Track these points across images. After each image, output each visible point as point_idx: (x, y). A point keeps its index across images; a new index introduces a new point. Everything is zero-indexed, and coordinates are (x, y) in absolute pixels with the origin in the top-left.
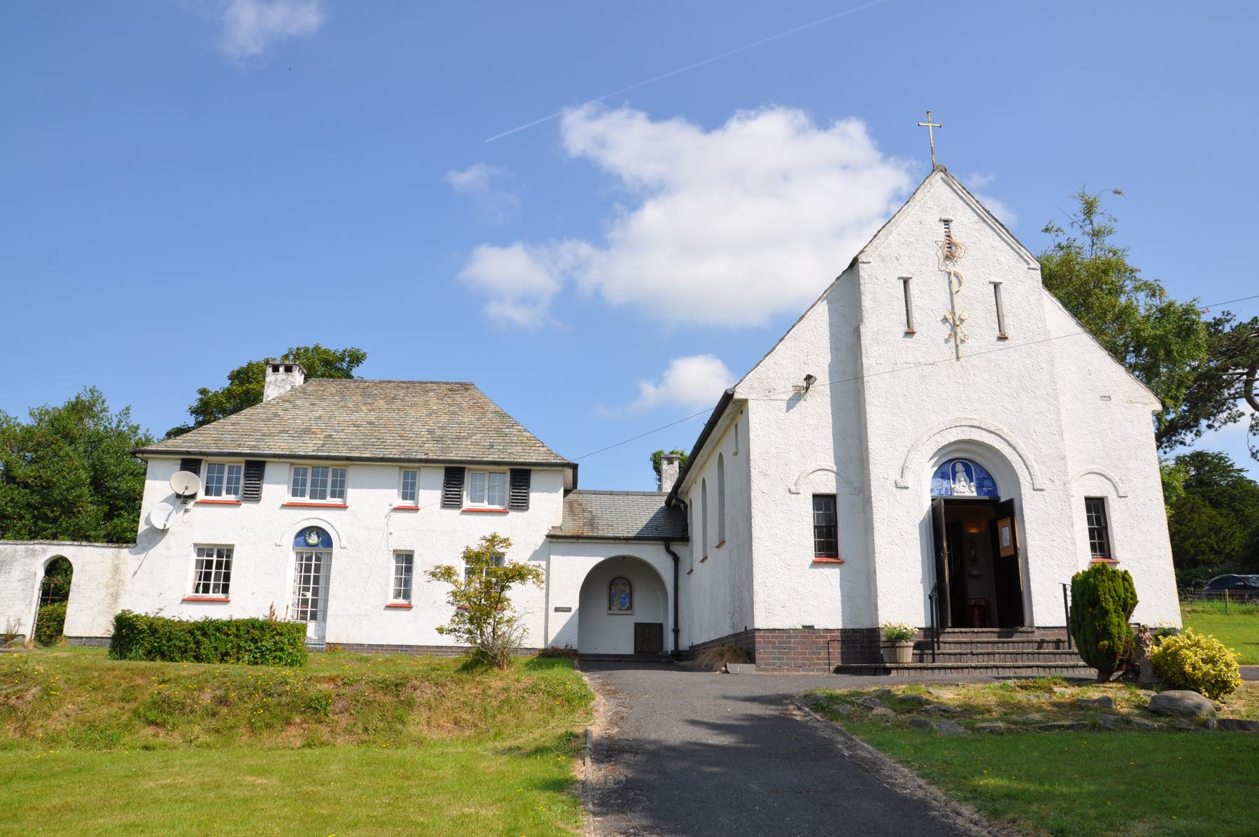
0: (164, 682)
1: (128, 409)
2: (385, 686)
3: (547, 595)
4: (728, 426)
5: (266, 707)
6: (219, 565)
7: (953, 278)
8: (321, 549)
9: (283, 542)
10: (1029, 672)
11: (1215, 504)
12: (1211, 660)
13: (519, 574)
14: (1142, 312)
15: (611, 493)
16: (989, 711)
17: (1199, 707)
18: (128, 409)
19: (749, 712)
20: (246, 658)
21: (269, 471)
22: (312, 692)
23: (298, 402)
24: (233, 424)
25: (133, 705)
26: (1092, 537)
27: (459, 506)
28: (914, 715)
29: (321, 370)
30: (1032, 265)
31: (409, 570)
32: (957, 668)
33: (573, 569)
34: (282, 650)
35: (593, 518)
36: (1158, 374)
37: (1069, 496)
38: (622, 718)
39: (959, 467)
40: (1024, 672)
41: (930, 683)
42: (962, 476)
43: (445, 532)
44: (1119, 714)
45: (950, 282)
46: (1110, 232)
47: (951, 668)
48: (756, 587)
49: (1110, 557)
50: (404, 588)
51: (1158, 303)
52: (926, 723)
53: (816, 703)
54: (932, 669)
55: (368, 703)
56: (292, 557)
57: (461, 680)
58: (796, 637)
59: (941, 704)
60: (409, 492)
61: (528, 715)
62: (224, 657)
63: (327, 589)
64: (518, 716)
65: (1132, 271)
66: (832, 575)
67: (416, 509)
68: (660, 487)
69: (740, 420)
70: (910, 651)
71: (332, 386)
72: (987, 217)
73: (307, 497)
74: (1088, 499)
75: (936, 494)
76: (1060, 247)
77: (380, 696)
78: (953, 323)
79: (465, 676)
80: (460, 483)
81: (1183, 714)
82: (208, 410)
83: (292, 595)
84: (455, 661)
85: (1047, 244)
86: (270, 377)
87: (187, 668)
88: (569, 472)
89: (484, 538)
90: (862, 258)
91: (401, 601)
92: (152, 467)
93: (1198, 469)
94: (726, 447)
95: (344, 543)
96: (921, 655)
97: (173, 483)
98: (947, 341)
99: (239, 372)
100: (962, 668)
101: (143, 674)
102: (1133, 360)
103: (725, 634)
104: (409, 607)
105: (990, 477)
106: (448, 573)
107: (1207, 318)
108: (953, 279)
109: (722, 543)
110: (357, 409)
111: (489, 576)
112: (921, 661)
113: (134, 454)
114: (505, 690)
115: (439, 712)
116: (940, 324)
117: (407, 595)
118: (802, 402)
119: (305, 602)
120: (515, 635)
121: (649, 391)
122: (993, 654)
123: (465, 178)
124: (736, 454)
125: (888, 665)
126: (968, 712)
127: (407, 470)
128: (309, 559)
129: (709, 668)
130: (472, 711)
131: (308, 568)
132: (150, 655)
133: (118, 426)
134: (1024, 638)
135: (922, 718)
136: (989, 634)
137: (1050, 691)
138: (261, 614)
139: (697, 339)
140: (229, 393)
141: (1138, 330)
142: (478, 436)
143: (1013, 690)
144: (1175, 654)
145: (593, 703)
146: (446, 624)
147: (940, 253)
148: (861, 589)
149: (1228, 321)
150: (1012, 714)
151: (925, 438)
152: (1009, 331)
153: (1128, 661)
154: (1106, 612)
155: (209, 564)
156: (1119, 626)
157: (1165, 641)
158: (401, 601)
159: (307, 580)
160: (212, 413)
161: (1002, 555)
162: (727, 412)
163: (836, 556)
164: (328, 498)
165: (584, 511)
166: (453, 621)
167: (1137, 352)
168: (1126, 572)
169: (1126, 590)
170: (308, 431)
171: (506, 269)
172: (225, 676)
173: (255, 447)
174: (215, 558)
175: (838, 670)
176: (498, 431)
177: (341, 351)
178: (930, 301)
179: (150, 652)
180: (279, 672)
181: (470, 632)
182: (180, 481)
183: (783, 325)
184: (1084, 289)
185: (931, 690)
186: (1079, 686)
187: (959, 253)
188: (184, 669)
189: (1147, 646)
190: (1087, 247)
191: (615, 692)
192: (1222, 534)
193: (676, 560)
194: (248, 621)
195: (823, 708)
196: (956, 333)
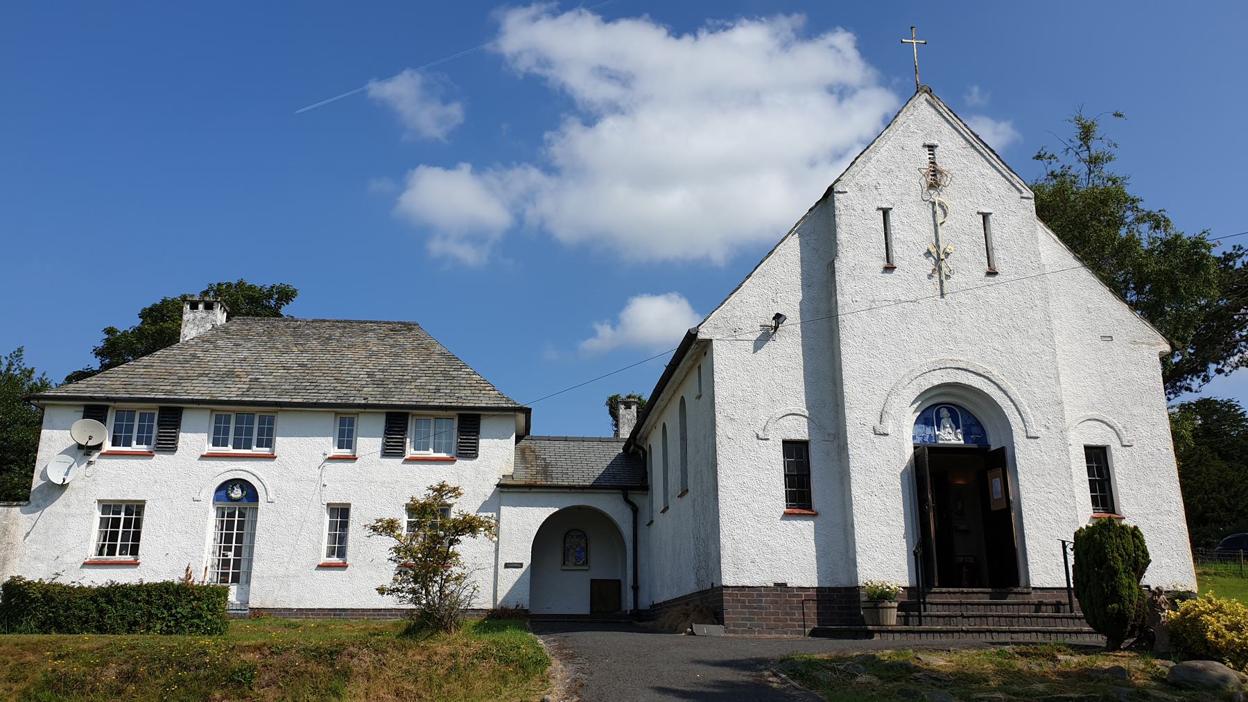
0: (61, 657)
1: (20, 350)
2: (318, 655)
3: (497, 550)
4: (691, 368)
5: (181, 682)
6: (127, 523)
7: (937, 208)
8: (245, 504)
9: (202, 497)
10: (1027, 638)
11: (1225, 457)
12: (1235, 627)
13: (469, 526)
14: (1145, 245)
15: (566, 439)
16: (986, 681)
17: (1225, 679)
18: (20, 350)
19: (715, 678)
20: (158, 626)
21: (187, 418)
22: (235, 663)
23: (220, 343)
24: (145, 367)
25: (22, 686)
26: (1092, 490)
27: (401, 455)
28: (902, 684)
29: (245, 308)
30: (1025, 195)
31: (344, 525)
32: (946, 632)
33: (524, 523)
34: (200, 617)
35: (546, 466)
36: (1163, 313)
37: (1066, 444)
38: (582, 685)
39: (944, 412)
40: (1027, 638)
41: (919, 649)
42: (947, 422)
43: (386, 483)
44: (1134, 686)
45: (934, 213)
46: (1110, 159)
47: (940, 632)
48: (723, 540)
49: (1114, 512)
50: (339, 546)
51: (1163, 235)
52: (916, 693)
53: (789, 666)
54: (920, 632)
55: (299, 674)
56: (212, 513)
57: (404, 646)
58: (768, 596)
59: (933, 671)
60: (346, 440)
61: (479, 684)
62: (132, 627)
63: (251, 548)
64: (467, 686)
65: (1133, 201)
66: (806, 527)
67: (353, 459)
68: (617, 433)
69: (703, 362)
70: (894, 612)
71: (258, 326)
72: (976, 142)
73: (230, 447)
74: (1088, 449)
75: (918, 441)
76: (1053, 175)
77: (312, 666)
78: (937, 257)
79: (408, 641)
80: (403, 430)
81: (1206, 688)
82: (116, 350)
83: (210, 556)
84: (395, 625)
85: (1040, 171)
86: (188, 314)
87: (89, 640)
88: (521, 417)
89: (431, 488)
90: (838, 187)
91: (335, 560)
92: (49, 414)
93: (1203, 417)
94: (689, 391)
95: (272, 496)
96: (907, 617)
97: (75, 432)
98: (930, 276)
99: (151, 309)
100: (953, 632)
101: (35, 648)
102: (1134, 298)
103: (689, 592)
104: (344, 566)
105: (978, 424)
106: (389, 527)
107: (1217, 252)
108: (938, 210)
109: (684, 492)
110: (287, 351)
111: (432, 534)
112: (906, 624)
113: (28, 400)
114: (453, 656)
115: (379, 682)
116: (923, 258)
117: (342, 553)
118: (771, 343)
119: (226, 563)
120: (465, 593)
121: (605, 331)
122: (986, 617)
123: (401, 90)
124: (699, 397)
125: (870, 627)
126: (962, 681)
127: (344, 419)
128: (232, 515)
129: (673, 630)
130: (416, 681)
131: (230, 525)
132: (43, 627)
133: (8, 370)
134: (1019, 599)
135: (912, 687)
136: (980, 595)
137: (1054, 659)
138: (176, 577)
139: (661, 277)
140: (139, 333)
141: (1140, 265)
142: (424, 379)
143: (1012, 657)
144: (1196, 619)
145: (549, 669)
146: (387, 582)
147: (923, 181)
148: (838, 543)
149: (1240, 256)
150: (1012, 683)
151: (907, 380)
152: (999, 266)
153: (1141, 628)
154: (1115, 572)
155: (116, 522)
156: (1130, 587)
157: (1182, 605)
158: (335, 560)
159: (228, 539)
160: (120, 355)
161: (993, 508)
162: (690, 353)
163: (809, 507)
164: (254, 447)
165: (537, 458)
166: (395, 580)
167: (1139, 289)
168: (1136, 528)
169: (1137, 547)
170: (231, 374)
171: (451, 198)
172: (133, 648)
173: (170, 391)
174: (122, 516)
175: (814, 633)
176: (445, 374)
177: (268, 287)
178: (912, 233)
179: (44, 624)
180: (197, 641)
181: (413, 591)
182: (82, 430)
183: (748, 260)
184: (1084, 220)
185: (920, 656)
186: (1086, 654)
187: (944, 181)
188: (85, 642)
189: (1163, 610)
190: (1083, 176)
191: (573, 656)
192: (1233, 490)
193: (635, 510)
194: (161, 585)
195: (802, 675)
196: (940, 268)
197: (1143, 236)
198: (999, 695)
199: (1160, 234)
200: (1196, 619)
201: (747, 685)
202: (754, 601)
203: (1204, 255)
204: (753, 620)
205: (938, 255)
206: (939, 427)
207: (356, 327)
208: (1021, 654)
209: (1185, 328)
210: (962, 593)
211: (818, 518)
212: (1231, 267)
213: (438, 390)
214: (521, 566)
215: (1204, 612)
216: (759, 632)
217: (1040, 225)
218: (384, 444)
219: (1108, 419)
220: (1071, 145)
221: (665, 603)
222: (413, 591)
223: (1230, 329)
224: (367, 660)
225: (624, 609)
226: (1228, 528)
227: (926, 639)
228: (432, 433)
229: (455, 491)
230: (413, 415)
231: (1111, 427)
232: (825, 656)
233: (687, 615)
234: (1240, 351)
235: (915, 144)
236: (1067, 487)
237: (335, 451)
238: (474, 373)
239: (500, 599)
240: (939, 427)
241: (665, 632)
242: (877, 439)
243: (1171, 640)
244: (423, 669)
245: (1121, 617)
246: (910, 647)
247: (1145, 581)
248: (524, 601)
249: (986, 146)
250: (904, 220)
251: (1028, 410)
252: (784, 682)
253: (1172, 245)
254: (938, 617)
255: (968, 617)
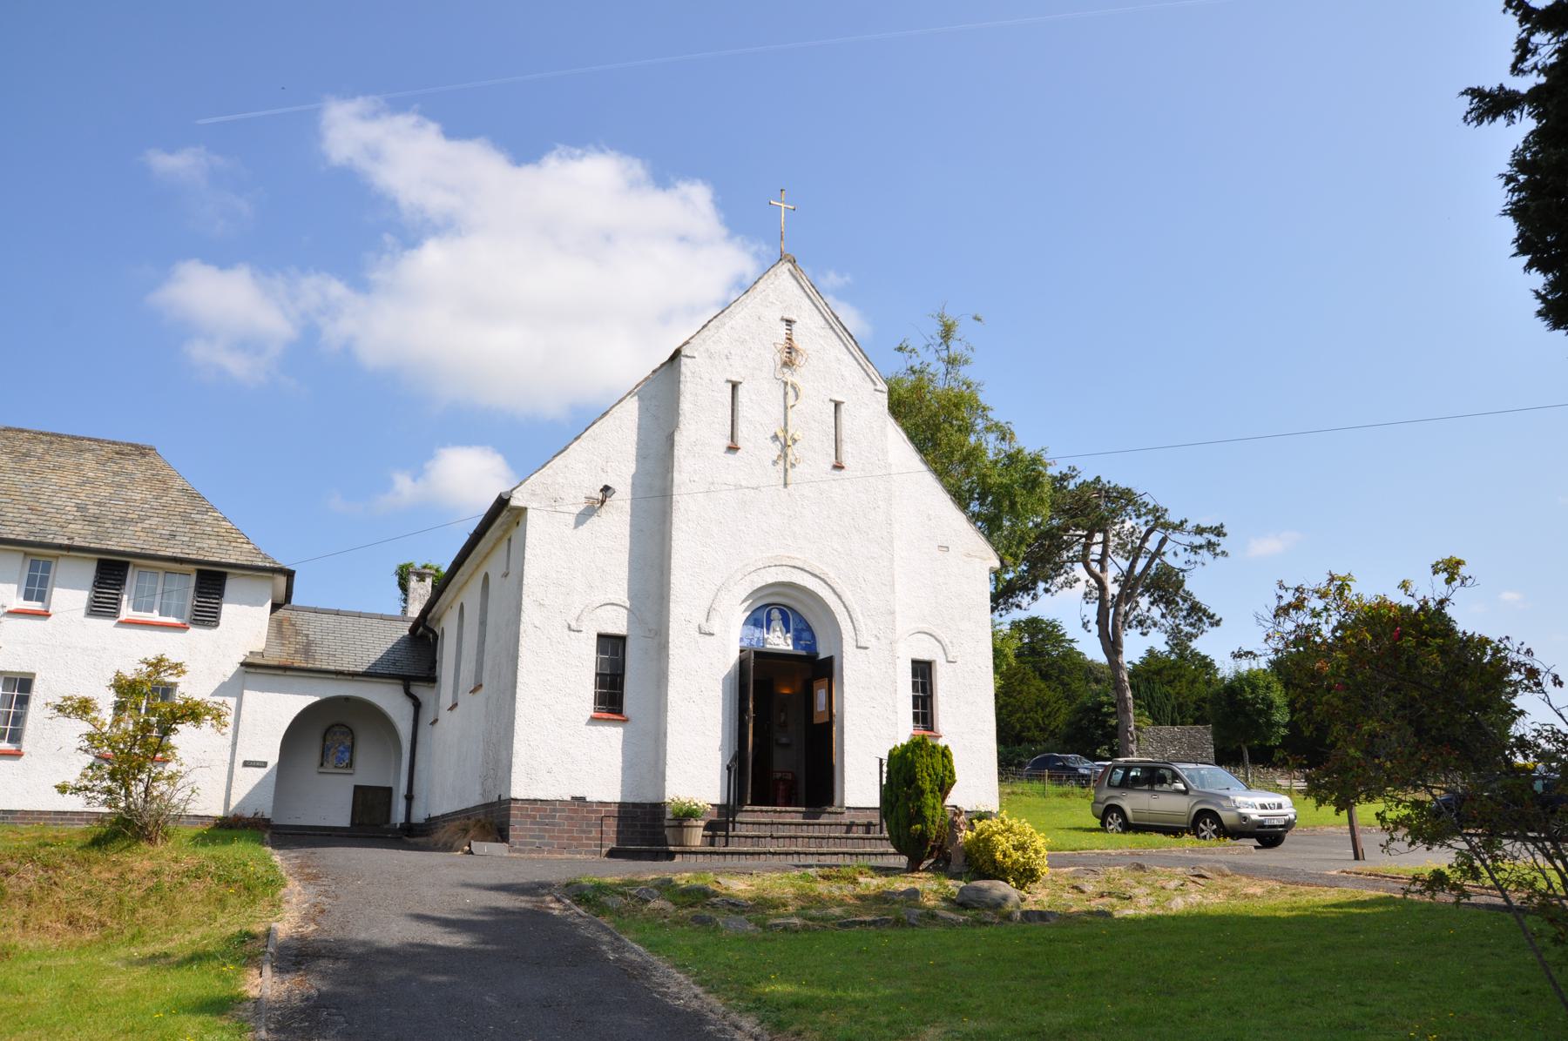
4: (500, 539)
11: (1045, 676)
13: (193, 713)
14: (991, 455)
15: (337, 613)
16: (785, 905)
17: (1005, 898)
26: (915, 706)
27: (114, 614)
31: (23, 701)
33: (273, 712)
35: (309, 644)
36: (1000, 528)
37: (895, 657)
38: (322, 911)
39: (776, 614)
40: (828, 860)
42: (777, 625)
46: (966, 362)
49: (932, 730)
52: (710, 919)
54: (724, 854)
57: (87, 860)
59: (731, 896)
60: (36, 588)
61: (186, 909)
64: (171, 911)
65: (984, 409)
66: (613, 735)
67: (45, 615)
68: (405, 610)
69: (514, 533)
70: (700, 832)
72: (835, 324)
78: (784, 442)
79: (94, 854)
80: (120, 582)
84: (84, 832)
85: (898, 365)
88: (281, 581)
89: (146, 662)
90: (686, 351)
93: (1031, 636)
94: (495, 566)
102: (977, 509)
105: (809, 628)
106: (84, 708)
107: (1053, 471)
109: (478, 687)
112: (712, 845)
114: (155, 873)
115: (44, 907)
116: (769, 442)
118: (595, 518)
120: (179, 795)
121: (404, 484)
124: (506, 575)
126: (761, 906)
129: (448, 848)
130: (99, 905)
136: (793, 815)
137: (855, 881)
141: (985, 475)
142: (154, 521)
143: (814, 880)
144: (988, 839)
145: (283, 891)
146: (72, 778)
147: (777, 358)
148: (647, 755)
152: (846, 460)
156: (934, 808)
157: (979, 825)
161: (816, 721)
162: (499, 521)
163: (620, 712)
165: (297, 633)
166: (84, 775)
167: (982, 499)
175: (612, 854)
176: (185, 517)
181: (109, 791)
184: (933, 422)
187: (799, 360)
190: (940, 376)
191: (316, 877)
193: (417, 705)
195: (588, 901)
198: (796, 921)
199: (1005, 446)
201: (524, 912)
202: (546, 817)
207: (68, 445)
209: (1018, 546)
213: (173, 536)
214: (264, 765)
216: (549, 852)
217: (891, 421)
218: (91, 600)
219: (941, 636)
222: (109, 791)
223: (1060, 548)
224: (31, 877)
228: (159, 591)
229: (178, 668)
230: (135, 566)
233: (465, 831)
235: (774, 316)
237: (20, 604)
238: (225, 519)
241: (439, 850)
244: (111, 889)
245: (922, 838)
247: (949, 801)
252: (567, 908)
253: (1013, 459)
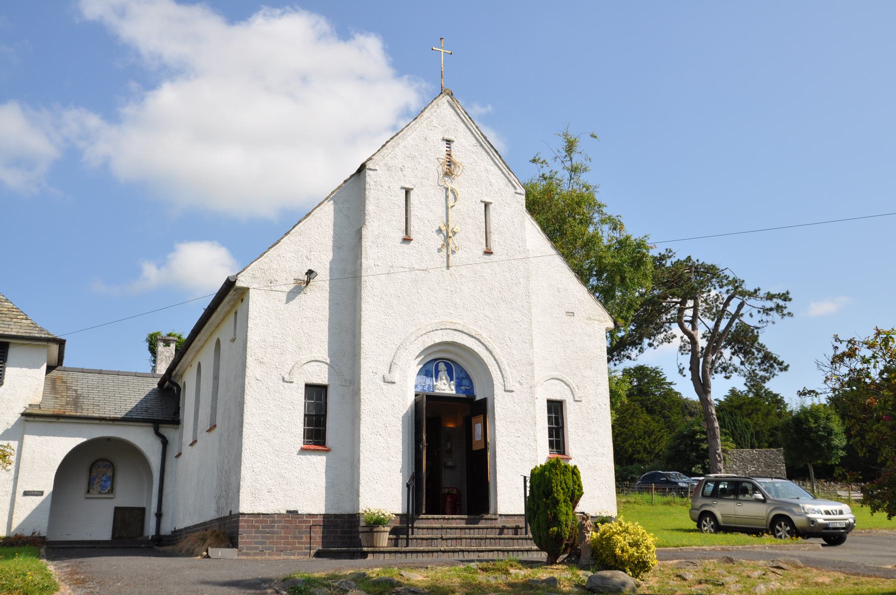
4: (228, 312)
7: (450, 193)
10: (490, 556)
11: (650, 411)
12: (635, 544)
14: (605, 242)
15: (100, 372)
26: (550, 435)
32: (427, 552)
35: (77, 397)
36: (613, 297)
37: (534, 398)
39: (442, 366)
40: (485, 556)
41: (402, 567)
42: (443, 375)
45: (447, 197)
46: (585, 170)
47: (422, 552)
49: (564, 453)
51: (618, 236)
54: (406, 552)
58: (280, 522)
59: (411, 585)
65: (600, 206)
66: (319, 461)
68: (154, 369)
70: (386, 536)
72: (484, 142)
75: (419, 390)
78: (447, 234)
85: (533, 173)
88: (55, 348)
90: (370, 165)
93: (639, 380)
94: (225, 333)
96: (396, 540)
98: (439, 250)
100: (432, 552)
102: (595, 283)
105: (468, 377)
107: (654, 253)
109: (213, 427)
112: (396, 545)
116: (435, 234)
118: (302, 295)
121: (150, 271)
122: (461, 539)
124: (233, 340)
125: (365, 549)
129: (190, 553)
136: (458, 521)
137: (507, 573)
141: (601, 257)
143: (476, 572)
144: (609, 539)
147: (440, 169)
148: (344, 477)
149: (669, 257)
151: (413, 337)
152: (494, 247)
153: (572, 546)
156: (567, 514)
157: (602, 528)
165: (68, 389)
167: (599, 275)
168: (575, 467)
169: (574, 482)
175: (318, 554)
178: (427, 212)
183: (291, 220)
184: (559, 216)
185: (403, 572)
186: (531, 568)
187: (457, 171)
189: (588, 532)
190: (566, 181)
191: (84, 581)
192: (653, 437)
193: (165, 442)
196: (448, 244)
197: (605, 234)
199: (616, 234)
200: (609, 539)
202: (267, 527)
203: (644, 254)
204: (265, 543)
205: (447, 233)
206: (436, 378)
208: (484, 570)
209: (629, 309)
210: (444, 519)
211: (330, 454)
212: (664, 265)
215: (616, 533)
216: (270, 554)
217: (528, 216)
219: (567, 378)
220: (558, 154)
221: (186, 529)
225: (146, 534)
226: (647, 466)
227: (411, 558)
231: (568, 385)
232: (323, 574)
234: (665, 330)
235: (436, 138)
236: (531, 433)
238: (7, 301)
239: (13, 530)
240: (436, 378)
242: (386, 387)
243: (592, 555)
245: (559, 537)
246: (395, 565)
247: (579, 509)
248: (42, 529)
249: (492, 147)
250: (422, 200)
251: (507, 368)
253: (622, 244)
254: (422, 539)
255: (446, 539)
